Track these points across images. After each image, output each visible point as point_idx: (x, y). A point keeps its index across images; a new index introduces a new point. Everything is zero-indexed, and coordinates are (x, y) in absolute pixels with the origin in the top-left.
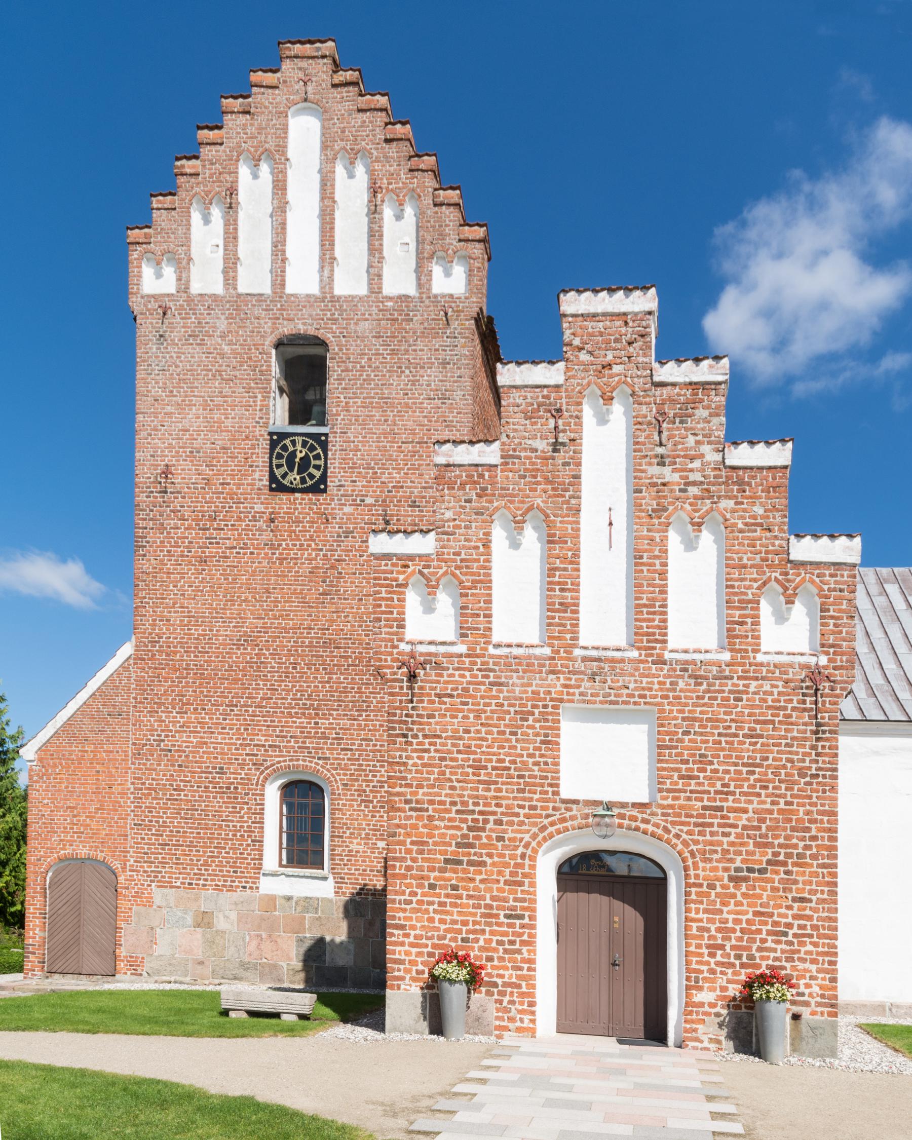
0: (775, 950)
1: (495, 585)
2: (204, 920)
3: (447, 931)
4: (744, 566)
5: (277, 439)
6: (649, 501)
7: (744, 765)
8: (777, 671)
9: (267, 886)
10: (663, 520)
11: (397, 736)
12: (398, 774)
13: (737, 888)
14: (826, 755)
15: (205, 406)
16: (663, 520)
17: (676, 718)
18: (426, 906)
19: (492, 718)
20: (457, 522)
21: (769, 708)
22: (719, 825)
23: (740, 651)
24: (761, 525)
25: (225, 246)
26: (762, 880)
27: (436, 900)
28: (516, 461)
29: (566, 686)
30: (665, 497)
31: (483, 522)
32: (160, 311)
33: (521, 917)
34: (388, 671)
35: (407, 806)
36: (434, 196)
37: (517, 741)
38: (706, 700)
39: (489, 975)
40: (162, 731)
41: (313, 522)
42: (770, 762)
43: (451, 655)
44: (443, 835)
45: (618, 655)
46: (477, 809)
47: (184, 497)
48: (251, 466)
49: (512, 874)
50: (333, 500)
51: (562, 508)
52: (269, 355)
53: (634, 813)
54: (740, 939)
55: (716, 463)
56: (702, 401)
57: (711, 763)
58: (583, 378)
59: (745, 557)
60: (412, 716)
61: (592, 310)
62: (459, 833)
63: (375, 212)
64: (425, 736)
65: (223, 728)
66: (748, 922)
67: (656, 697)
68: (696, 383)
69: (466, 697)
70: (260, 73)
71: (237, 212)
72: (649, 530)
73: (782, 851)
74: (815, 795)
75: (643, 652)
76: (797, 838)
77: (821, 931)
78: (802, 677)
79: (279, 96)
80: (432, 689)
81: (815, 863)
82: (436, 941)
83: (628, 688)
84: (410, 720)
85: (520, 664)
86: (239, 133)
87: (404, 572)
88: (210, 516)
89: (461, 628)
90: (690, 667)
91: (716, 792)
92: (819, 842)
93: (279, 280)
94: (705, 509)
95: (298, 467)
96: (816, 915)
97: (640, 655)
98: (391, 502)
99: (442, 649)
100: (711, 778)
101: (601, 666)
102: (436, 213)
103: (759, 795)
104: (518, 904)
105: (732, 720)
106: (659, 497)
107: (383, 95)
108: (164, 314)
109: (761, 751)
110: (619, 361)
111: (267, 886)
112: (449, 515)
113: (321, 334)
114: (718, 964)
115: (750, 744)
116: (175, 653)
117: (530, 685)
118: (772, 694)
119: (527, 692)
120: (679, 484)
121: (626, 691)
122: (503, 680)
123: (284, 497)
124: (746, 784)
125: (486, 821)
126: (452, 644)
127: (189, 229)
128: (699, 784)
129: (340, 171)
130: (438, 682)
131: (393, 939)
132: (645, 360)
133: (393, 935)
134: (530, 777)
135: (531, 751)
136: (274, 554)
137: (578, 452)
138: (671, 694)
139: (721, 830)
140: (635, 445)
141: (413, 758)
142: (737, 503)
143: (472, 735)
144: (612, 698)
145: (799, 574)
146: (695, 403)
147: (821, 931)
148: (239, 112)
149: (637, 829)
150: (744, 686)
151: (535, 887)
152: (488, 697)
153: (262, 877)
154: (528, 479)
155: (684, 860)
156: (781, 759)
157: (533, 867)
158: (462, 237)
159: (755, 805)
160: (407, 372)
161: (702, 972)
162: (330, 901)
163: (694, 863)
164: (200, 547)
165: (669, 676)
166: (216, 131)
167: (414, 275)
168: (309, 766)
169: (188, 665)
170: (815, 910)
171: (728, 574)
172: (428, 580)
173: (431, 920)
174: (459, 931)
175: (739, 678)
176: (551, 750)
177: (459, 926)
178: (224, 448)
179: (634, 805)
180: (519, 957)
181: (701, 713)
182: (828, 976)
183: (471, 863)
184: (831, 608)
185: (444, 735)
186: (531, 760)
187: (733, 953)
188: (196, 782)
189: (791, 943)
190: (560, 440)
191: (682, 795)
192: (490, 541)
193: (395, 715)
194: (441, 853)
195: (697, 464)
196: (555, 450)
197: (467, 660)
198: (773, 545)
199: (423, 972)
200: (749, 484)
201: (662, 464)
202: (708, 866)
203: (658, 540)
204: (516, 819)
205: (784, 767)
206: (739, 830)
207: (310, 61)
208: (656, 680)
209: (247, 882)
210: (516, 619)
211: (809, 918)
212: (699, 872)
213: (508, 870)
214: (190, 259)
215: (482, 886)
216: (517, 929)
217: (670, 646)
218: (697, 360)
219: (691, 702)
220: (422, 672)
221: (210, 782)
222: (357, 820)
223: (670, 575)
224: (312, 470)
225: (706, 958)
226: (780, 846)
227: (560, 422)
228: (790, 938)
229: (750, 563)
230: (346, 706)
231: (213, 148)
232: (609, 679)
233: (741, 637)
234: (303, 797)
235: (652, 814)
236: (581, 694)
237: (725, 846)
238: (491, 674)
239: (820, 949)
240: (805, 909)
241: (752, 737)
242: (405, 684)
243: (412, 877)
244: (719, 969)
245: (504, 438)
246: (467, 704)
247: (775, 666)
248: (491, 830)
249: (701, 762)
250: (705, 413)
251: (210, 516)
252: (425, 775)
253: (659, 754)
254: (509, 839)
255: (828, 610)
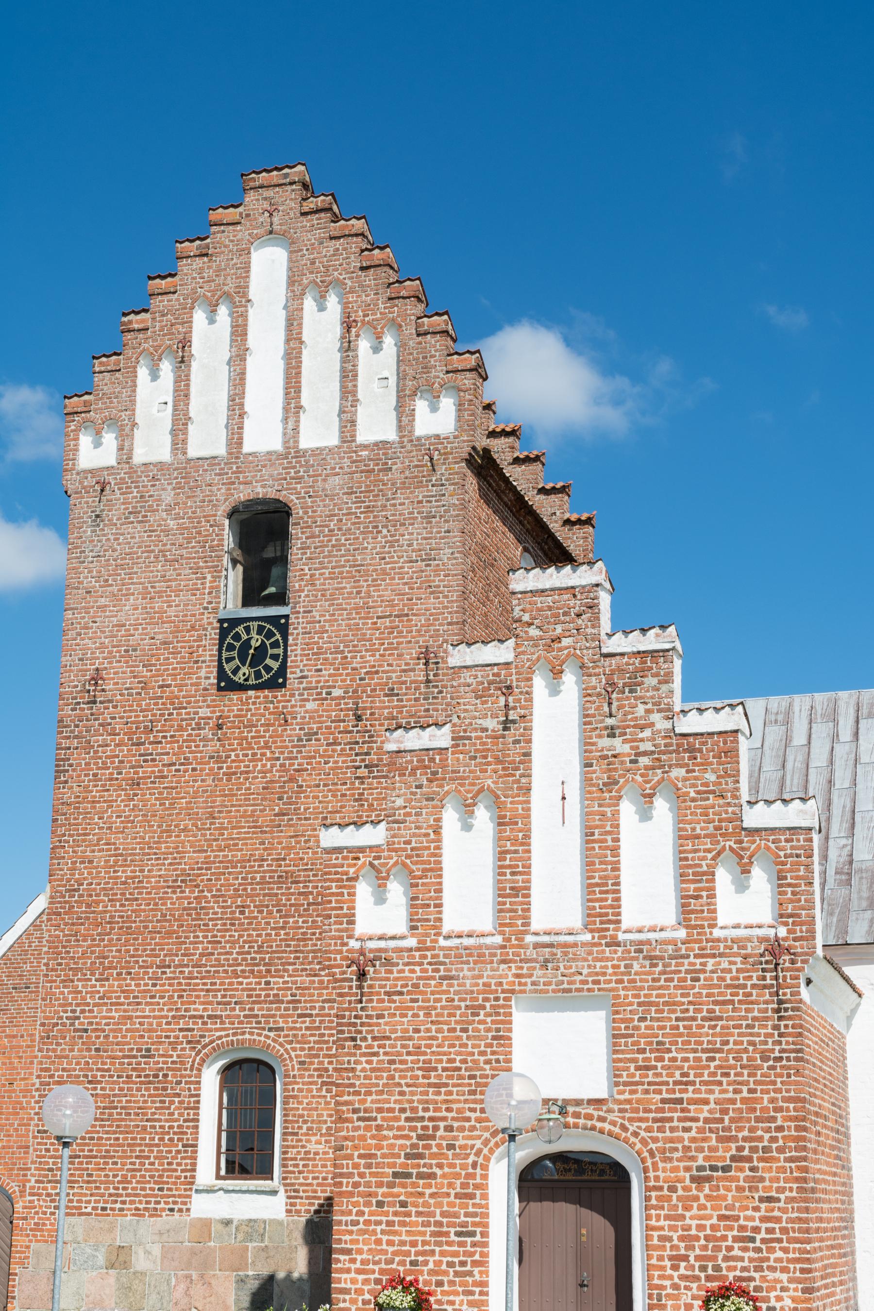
0: (742, 1259)
1: (445, 873)
2: (119, 1258)
3: (395, 1253)
4: (698, 837)
5: (228, 627)
6: (600, 776)
7: (704, 1051)
8: (735, 946)
9: (203, 1206)
10: (614, 794)
11: (346, 1039)
12: (346, 1081)
13: (700, 1189)
14: (790, 1035)
15: (145, 594)
16: (614, 794)
17: (631, 1004)
18: (373, 1227)
19: (442, 1015)
20: (408, 810)
21: (728, 986)
22: (680, 1120)
23: (695, 927)
24: (713, 792)
25: (175, 406)
26: (726, 1179)
27: (384, 1219)
28: (467, 742)
29: (517, 976)
30: (616, 770)
31: (434, 807)
32: (98, 488)
33: (472, 1234)
34: (337, 970)
35: (355, 1116)
36: (418, 326)
37: (468, 1038)
38: (662, 982)
39: (439, 1302)
40: (78, 1005)
41: (268, 725)
42: (731, 1046)
43: (401, 950)
44: (392, 1146)
45: (570, 939)
46: (427, 1115)
47: (115, 707)
48: (197, 662)
49: (464, 1186)
50: (293, 695)
51: (512, 788)
52: (221, 526)
53: (590, 1110)
54: (704, 1248)
55: (667, 730)
56: (651, 668)
57: (669, 1051)
58: (533, 654)
59: (698, 827)
60: (360, 1017)
61: (540, 586)
62: (408, 1143)
63: (349, 349)
64: (374, 1039)
65: (152, 997)
66: (713, 1228)
67: (610, 981)
68: (644, 652)
69: (416, 993)
70: (220, 210)
71: (190, 366)
72: (600, 805)
73: (747, 1145)
74: (779, 1080)
75: (596, 935)
76: (763, 1129)
77: (791, 1234)
78: (761, 951)
79: (242, 233)
80: (381, 987)
81: (782, 1156)
82: (383, 1266)
83: (581, 974)
84: (358, 1021)
85: (471, 955)
86: (195, 278)
87: (355, 865)
88: (146, 727)
89: (411, 920)
90: (645, 948)
91: (676, 1083)
92: (786, 1133)
93: (235, 439)
94: (656, 779)
95: (253, 658)
96: (785, 1216)
97: (593, 938)
98: (364, 691)
99: (392, 944)
100: (669, 1068)
101: (554, 951)
102: (420, 343)
103: (720, 1083)
104: (469, 1219)
105: (690, 1003)
106: (610, 770)
107: (359, 219)
108: (102, 491)
109: (721, 1035)
110: (568, 634)
111: (203, 1206)
112: (400, 802)
113: (282, 496)
114: (682, 1277)
115: (710, 1027)
116: (97, 903)
117: (481, 977)
118: (730, 971)
119: (477, 985)
120: (629, 755)
121: (578, 978)
122: (454, 973)
123: (235, 696)
124: (706, 1072)
125: (436, 1128)
126: (402, 938)
127: (134, 391)
128: (657, 1075)
129: (309, 304)
130: (388, 979)
131: (339, 1265)
132: (593, 631)
133: (339, 1261)
134: (482, 1076)
135: (482, 1048)
136: (220, 768)
137: (528, 729)
138: (626, 978)
139: (681, 1124)
140: (586, 718)
141: (361, 1063)
142: (688, 772)
143: (422, 1034)
144: (565, 986)
145: (754, 842)
146: (644, 671)
147: (791, 1234)
148: (195, 256)
149: (593, 1128)
150: (701, 964)
151: (487, 1199)
152: (438, 993)
153: (194, 1195)
154: (478, 760)
155: (643, 1161)
156: (742, 1043)
157: (485, 1177)
158: (450, 368)
159: (717, 1095)
160: (385, 531)
161: (663, 1288)
162: (280, 1223)
163: (653, 1164)
164: (132, 767)
165: (624, 959)
166: (169, 279)
167: (394, 414)
168: (257, 1040)
169: (112, 917)
170: (784, 1211)
171: (682, 846)
172: (378, 871)
173: (378, 1242)
174: (408, 1253)
175: (696, 956)
176: (502, 1045)
177: (408, 1248)
178: (165, 643)
179: (590, 1102)
180: (470, 1279)
181: (658, 996)
182: (800, 1286)
183: (420, 1176)
184: (788, 875)
185: (393, 1036)
186: (482, 1058)
187: (697, 1264)
188: (116, 1070)
189: (758, 1250)
190: (510, 718)
191: (640, 1087)
192: (441, 827)
193: (343, 1017)
194: (390, 1165)
195: (647, 733)
196: (505, 729)
197: (417, 954)
198: (727, 813)
199: (369, 1302)
200: (700, 751)
201: (612, 735)
202: (669, 1166)
203: (609, 815)
204: (467, 1124)
205: (746, 1051)
206: (700, 1124)
207: (277, 189)
208: (609, 964)
209: (175, 1203)
210: (468, 904)
211: (778, 1220)
212: (659, 1173)
213: (458, 1182)
214: (134, 425)
215: (432, 1201)
216: (469, 1248)
217: (624, 926)
218: (644, 631)
219: (646, 985)
220: (372, 969)
221: (133, 1069)
222: (316, 1109)
223: (623, 851)
224: (269, 661)
225: (669, 1272)
226: (745, 1139)
227: (511, 699)
228: (758, 1244)
229: (703, 832)
230: (305, 958)
231: (165, 298)
232: (561, 965)
233: (697, 912)
234: (250, 1081)
235: (609, 1111)
236: (534, 983)
237: (686, 1143)
238: (442, 968)
239: (791, 1256)
240: (773, 1210)
241: (711, 1019)
242: (355, 983)
243: (360, 1194)
244: (683, 1284)
245: (455, 720)
246: (416, 1001)
247: (733, 941)
248: (442, 1138)
249: (658, 1050)
250: (654, 681)
251: (146, 727)
252: (374, 1081)
253: (615, 1044)
254: (460, 1147)
255: (785, 878)
